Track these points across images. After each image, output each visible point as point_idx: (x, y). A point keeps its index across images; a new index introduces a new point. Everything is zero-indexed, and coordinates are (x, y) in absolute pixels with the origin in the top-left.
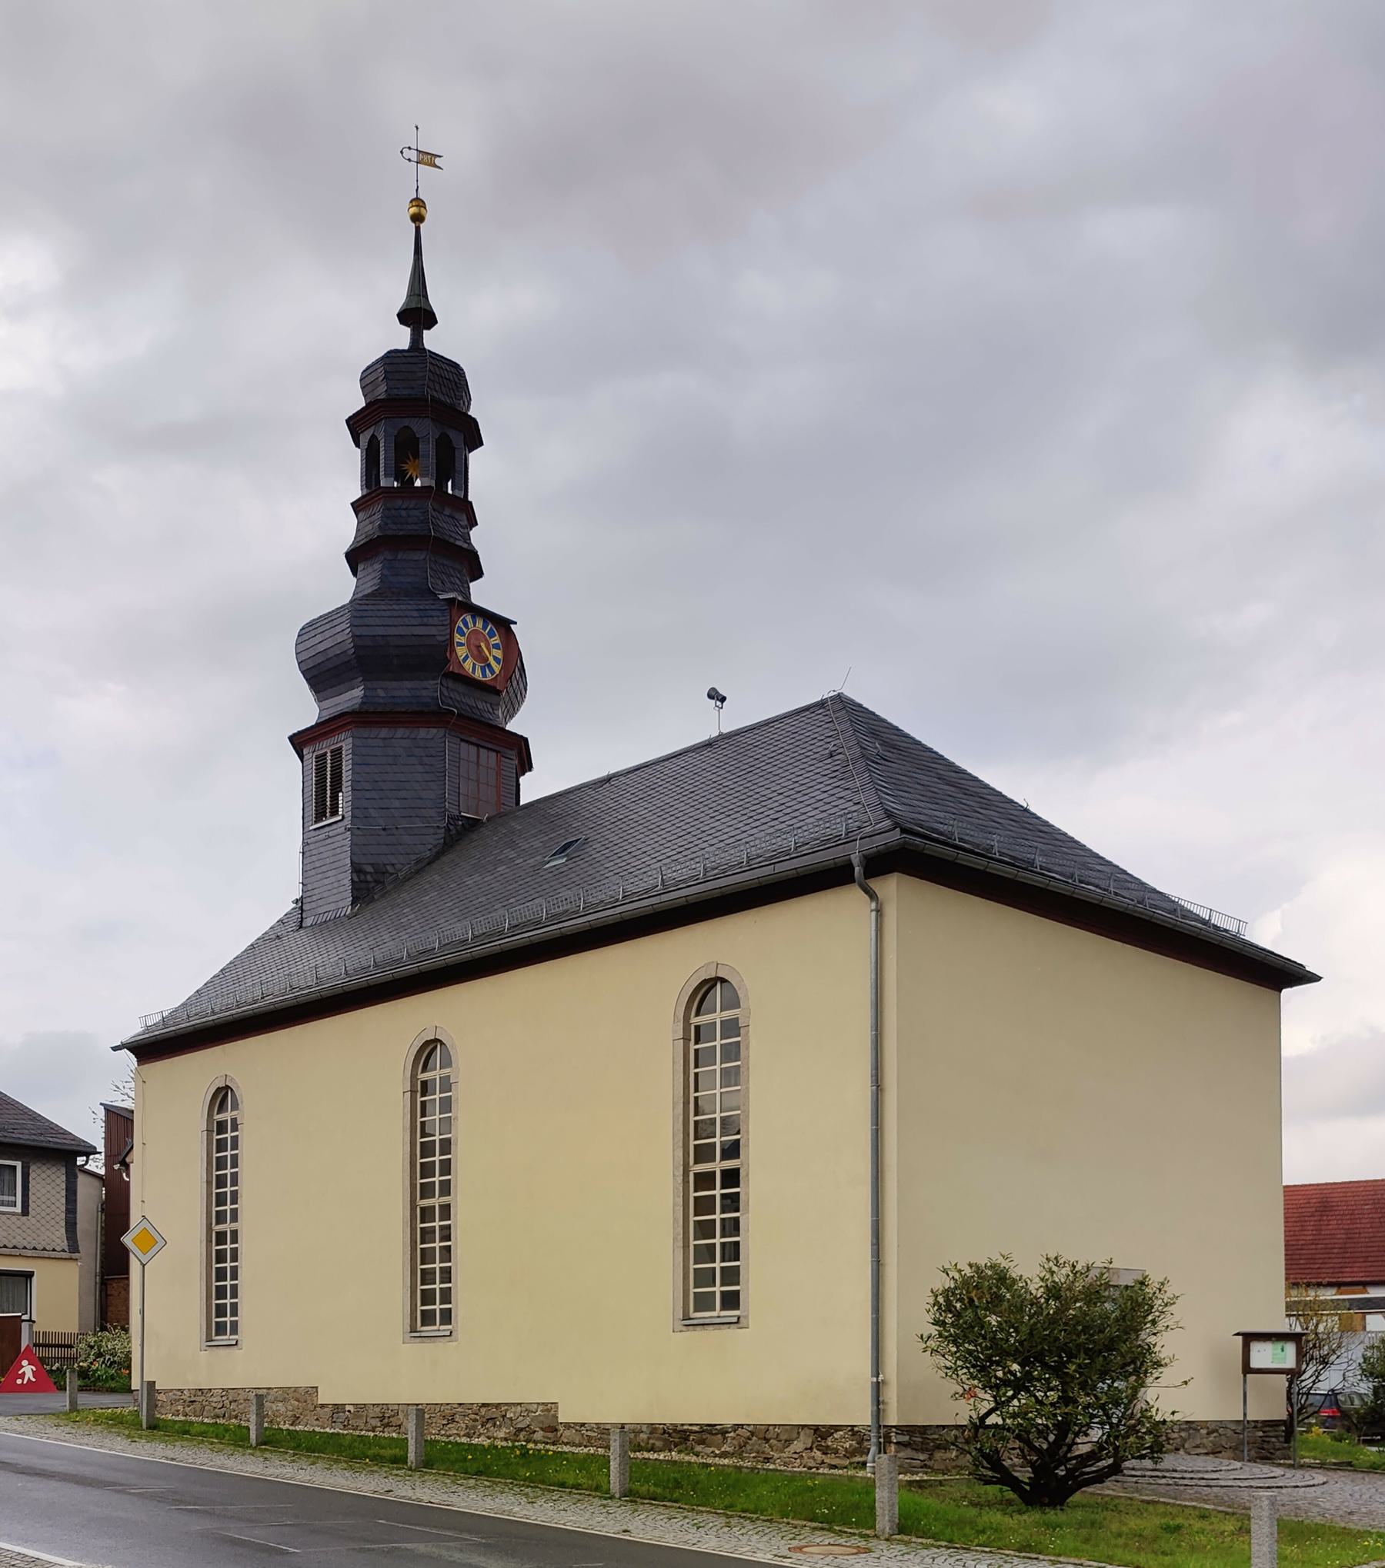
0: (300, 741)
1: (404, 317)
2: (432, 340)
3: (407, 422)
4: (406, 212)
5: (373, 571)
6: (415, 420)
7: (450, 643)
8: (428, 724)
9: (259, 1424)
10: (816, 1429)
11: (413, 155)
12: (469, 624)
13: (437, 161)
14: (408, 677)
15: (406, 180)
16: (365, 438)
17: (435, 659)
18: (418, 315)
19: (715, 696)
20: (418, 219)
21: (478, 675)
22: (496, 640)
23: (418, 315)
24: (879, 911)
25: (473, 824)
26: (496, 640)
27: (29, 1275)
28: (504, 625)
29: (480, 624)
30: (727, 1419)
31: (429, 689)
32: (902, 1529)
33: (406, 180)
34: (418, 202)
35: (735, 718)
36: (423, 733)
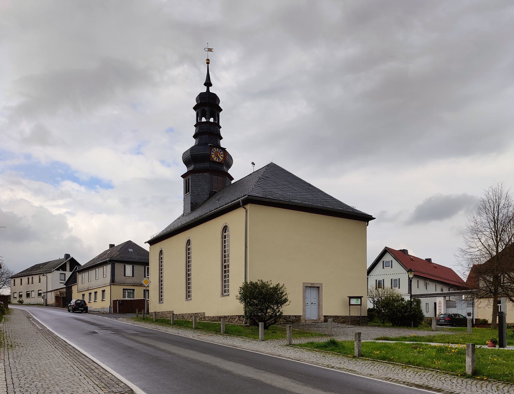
0: (183, 176)
1: (205, 84)
2: (212, 90)
3: (203, 108)
4: (205, 62)
6: (208, 105)
7: (211, 155)
8: (206, 172)
9: (155, 318)
10: (239, 316)
11: (207, 50)
12: (215, 150)
14: (206, 163)
15: (206, 55)
17: (207, 158)
18: (208, 84)
19: (253, 164)
20: (208, 63)
21: (217, 161)
22: (222, 153)
23: (208, 84)
24: (246, 212)
25: (215, 192)
26: (222, 153)
27: (134, 290)
28: (386, 251)
29: (218, 150)
30: (227, 315)
31: (207, 165)
32: (225, 333)
33: (206, 55)
34: (208, 60)
35: (257, 167)
36: (205, 174)
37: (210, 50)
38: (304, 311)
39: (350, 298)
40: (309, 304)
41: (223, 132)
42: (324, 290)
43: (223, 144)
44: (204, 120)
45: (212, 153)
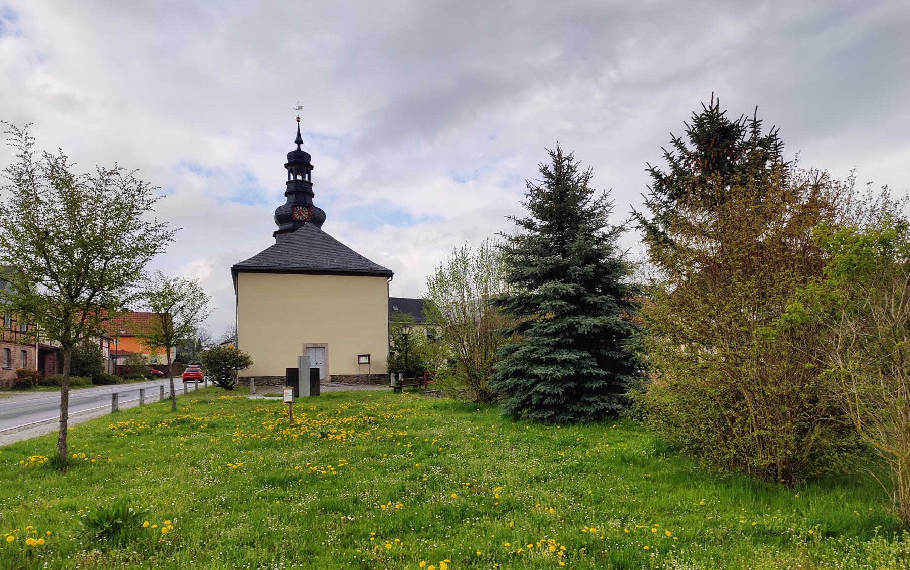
2: (304, 148)
5: (293, 197)
6: (299, 162)
18: (299, 141)
23: (299, 141)
34: (298, 118)
37: (300, 108)
39: (359, 356)
41: (314, 189)
42: (330, 350)
43: (316, 201)
44: (299, 178)
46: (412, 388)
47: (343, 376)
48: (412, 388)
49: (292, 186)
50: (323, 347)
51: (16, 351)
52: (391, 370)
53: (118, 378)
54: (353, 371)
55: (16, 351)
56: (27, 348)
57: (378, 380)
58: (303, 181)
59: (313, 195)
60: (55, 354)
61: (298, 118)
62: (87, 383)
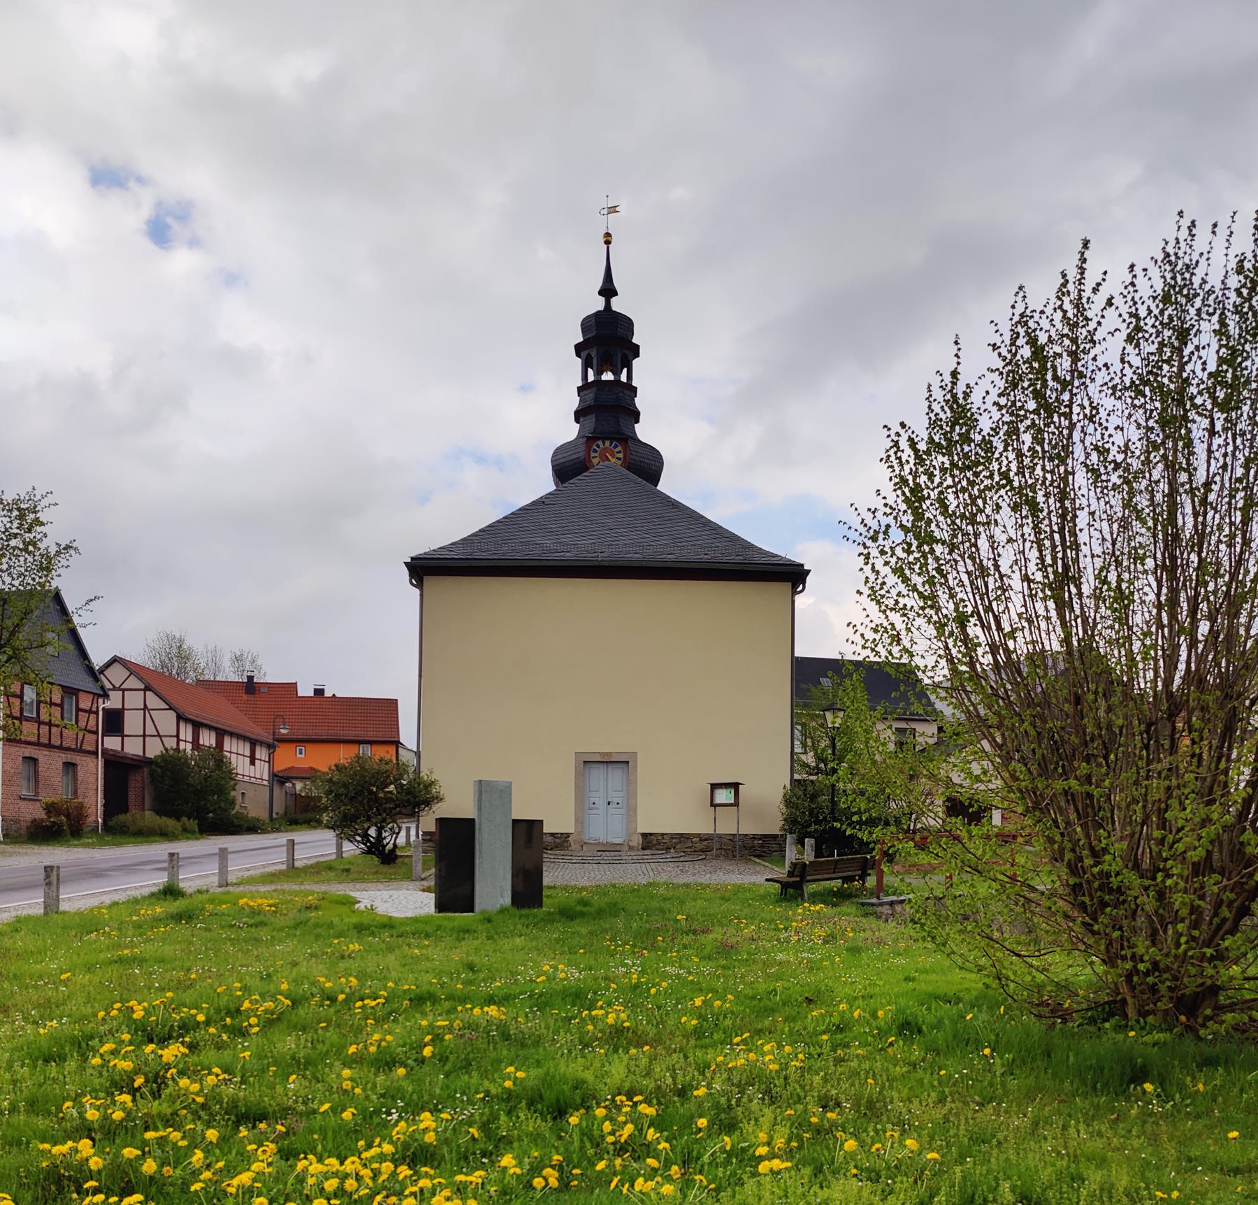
2: (617, 305)
4: (602, 240)
5: (591, 421)
6: (608, 340)
13: (1049, 328)
16: (584, 354)
18: (608, 291)
20: (608, 243)
22: (619, 448)
23: (608, 291)
28: (115, 660)
34: (608, 235)
38: (579, 821)
39: (714, 786)
40: (601, 803)
41: (639, 402)
42: (643, 769)
43: (644, 431)
44: (608, 376)
45: (593, 454)
46: (836, 884)
47: (673, 836)
48: (836, 884)
49: (590, 395)
50: (623, 763)
51: (51, 763)
52: (792, 823)
53: (170, 823)
54: (696, 822)
55: (51, 763)
56: (42, 755)
57: (759, 848)
58: (617, 382)
59: (636, 416)
60: (146, 770)
61: (608, 235)
62: (185, 830)
